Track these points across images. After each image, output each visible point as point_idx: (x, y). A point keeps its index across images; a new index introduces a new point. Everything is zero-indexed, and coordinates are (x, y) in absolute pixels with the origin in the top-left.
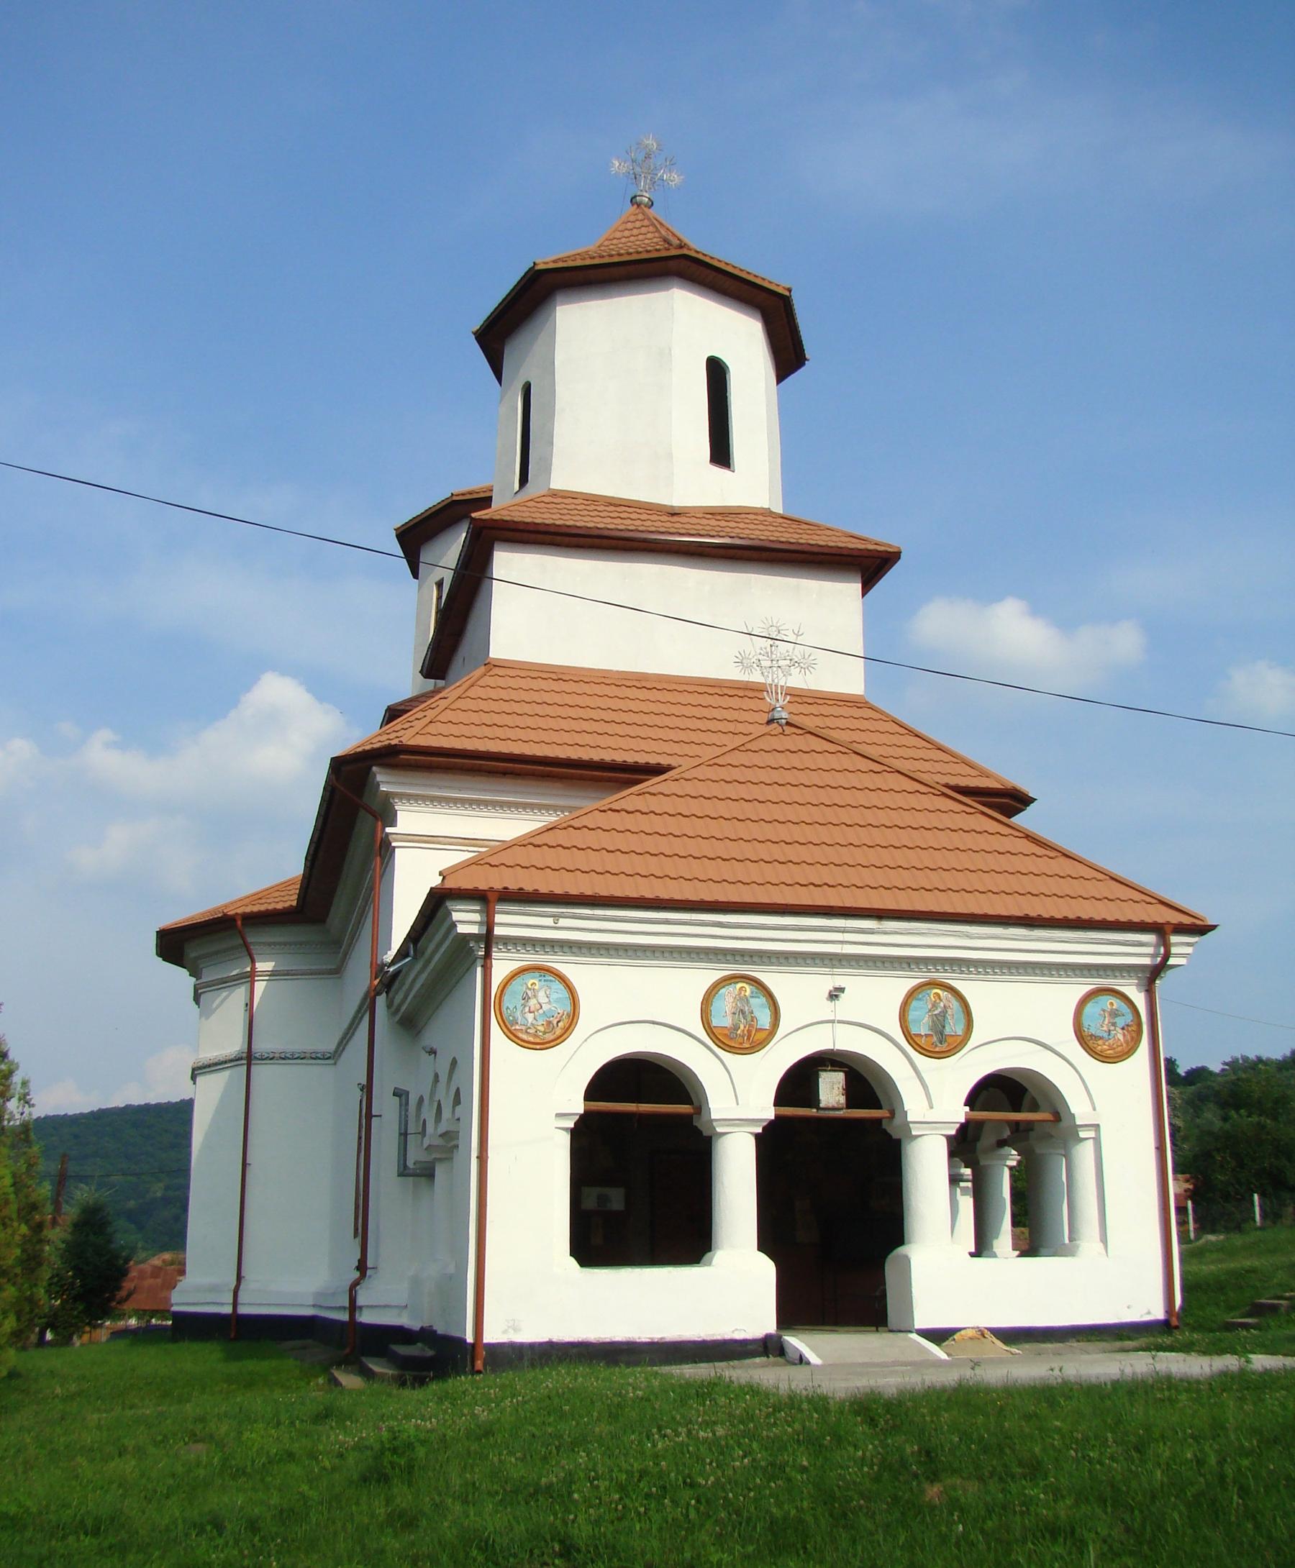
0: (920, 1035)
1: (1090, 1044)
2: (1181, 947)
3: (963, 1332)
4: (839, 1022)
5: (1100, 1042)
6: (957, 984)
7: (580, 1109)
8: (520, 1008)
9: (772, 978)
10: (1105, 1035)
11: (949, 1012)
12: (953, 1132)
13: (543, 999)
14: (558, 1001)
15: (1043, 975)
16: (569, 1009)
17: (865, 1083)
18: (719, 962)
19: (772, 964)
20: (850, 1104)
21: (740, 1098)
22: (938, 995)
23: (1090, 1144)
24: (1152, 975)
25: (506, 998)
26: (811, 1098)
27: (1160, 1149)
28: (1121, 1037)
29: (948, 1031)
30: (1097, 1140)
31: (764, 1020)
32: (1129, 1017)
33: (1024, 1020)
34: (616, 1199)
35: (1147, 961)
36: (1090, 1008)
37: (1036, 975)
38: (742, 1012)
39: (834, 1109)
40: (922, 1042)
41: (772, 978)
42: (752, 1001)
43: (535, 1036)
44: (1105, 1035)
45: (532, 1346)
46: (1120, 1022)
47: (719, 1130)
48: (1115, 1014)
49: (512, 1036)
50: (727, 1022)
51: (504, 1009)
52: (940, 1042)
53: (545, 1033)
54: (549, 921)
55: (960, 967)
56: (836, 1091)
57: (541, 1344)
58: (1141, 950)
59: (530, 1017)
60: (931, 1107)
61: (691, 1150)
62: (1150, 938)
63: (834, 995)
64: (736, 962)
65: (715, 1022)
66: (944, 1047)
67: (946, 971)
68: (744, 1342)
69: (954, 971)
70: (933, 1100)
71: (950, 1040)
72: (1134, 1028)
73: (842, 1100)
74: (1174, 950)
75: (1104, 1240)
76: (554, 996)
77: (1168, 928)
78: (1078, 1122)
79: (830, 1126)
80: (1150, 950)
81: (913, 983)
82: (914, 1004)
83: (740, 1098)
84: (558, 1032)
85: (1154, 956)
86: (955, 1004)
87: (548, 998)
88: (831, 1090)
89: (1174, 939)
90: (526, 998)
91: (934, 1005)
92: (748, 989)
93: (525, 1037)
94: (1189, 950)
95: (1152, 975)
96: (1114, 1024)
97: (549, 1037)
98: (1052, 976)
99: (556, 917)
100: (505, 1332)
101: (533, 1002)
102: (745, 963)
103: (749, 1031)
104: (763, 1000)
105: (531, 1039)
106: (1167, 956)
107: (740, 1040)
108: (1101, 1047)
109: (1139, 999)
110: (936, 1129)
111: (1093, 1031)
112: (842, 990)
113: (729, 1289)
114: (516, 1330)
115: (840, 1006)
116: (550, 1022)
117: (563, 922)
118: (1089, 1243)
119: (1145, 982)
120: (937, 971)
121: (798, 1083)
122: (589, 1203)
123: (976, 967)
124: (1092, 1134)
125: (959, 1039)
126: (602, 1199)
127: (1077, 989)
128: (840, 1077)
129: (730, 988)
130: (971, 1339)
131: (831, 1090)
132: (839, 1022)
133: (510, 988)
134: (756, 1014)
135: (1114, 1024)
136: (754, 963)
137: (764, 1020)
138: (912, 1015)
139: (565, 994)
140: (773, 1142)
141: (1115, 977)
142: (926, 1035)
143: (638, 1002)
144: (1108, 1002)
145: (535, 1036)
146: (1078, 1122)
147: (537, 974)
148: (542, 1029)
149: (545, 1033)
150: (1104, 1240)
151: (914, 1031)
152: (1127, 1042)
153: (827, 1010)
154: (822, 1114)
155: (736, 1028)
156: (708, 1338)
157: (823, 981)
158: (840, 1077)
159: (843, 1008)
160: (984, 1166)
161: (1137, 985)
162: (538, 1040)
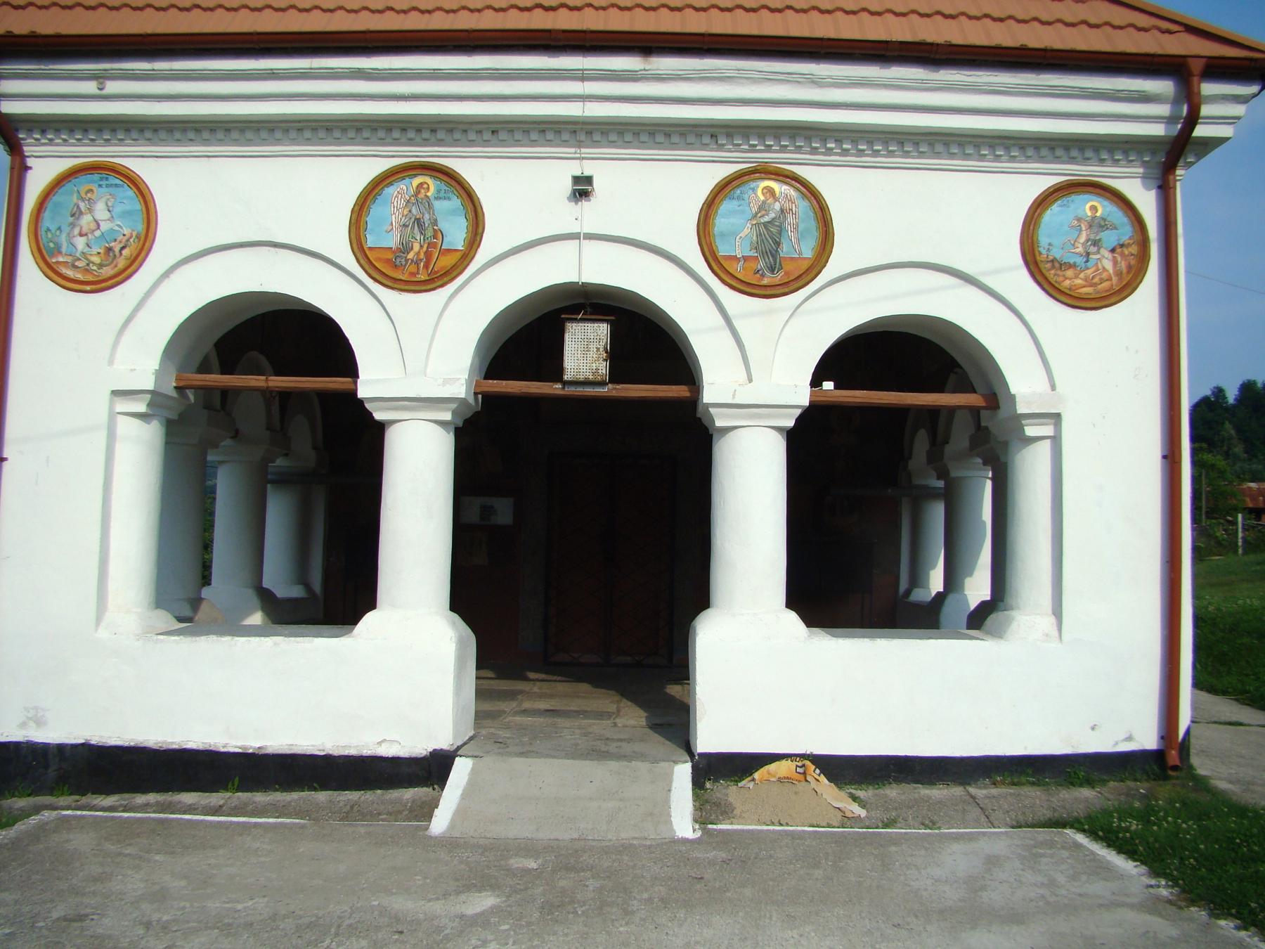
0: (734, 258)
1: (1051, 275)
2: (1225, 109)
3: (773, 767)
4: (590, 237)
5: (1070, 273)
6: (134, 165)
7: (802, 397)
8: (66, 229)
9: (475, 169)
10: (1080, 261)
11: (790, 219)
12: (790, 423)
13: (101, 211)
14: (127, 214)
15: (967, 157)
16: (141, 227)
17: (647, 341)
18: (382, 142)
19: (471, 143)
20: (616, 376)
21: (416, 363)
22: (770, 191)
23: (1044, 448)
24: (1173, 154)
25: (47, 215)
26: (551, 364)
27: (1171, 458)
28: (1108, 265)
29: (785, 250)
30: (1056, 440)
31: (456, 234)
32: (1125, 231)
33: (930, 236)
34: (503, 511)
35: (1158, 130)
36: (1054, 215)
37: (952, 156)
38: (418, 221)
39: (586, 383)
40: (738, 269)
41: (475, 169)
42: (437, 205)
43: (87, 271)
44: (1080, 261)
45: (61, 748)
46: (1110, 238)
47: (718, 423)
48: (1099, 225)
49: (52, 271)
50: (392, 241)
51: (42, 232)
52: (772, 270)
53: (101, 266)
54: (90, 87)
55: (824, 141)
56: (593, 354)
57: (75, 747)
58: (1143, 109)
59: (80, 243)
60: (750, 380)
61: (347, 449)
62: (1163, 86)
63: (582, 189)
64: (411, 142)
65: (371, 241)
66: (779, 277)
67: (783, 149)
68: (395, 761)
69: (798, 149)
70: (757, 372)
71: (788, 266)
72: (1134, 249)
73: (603, 368)
74: (1205, 110)
75: (1057, 612)
76: (119, 209)
77: (1196, 66)
78: (1021, 409)
79: (584, 411)
80: (1164, 110)
81: (723, 171)
82: (726, 207)
83: (416, 363)
84: (121, 263)
85: (1170, 120)
86: (803, 207)
87: (106, 213)
88: (585, 351)
89: (1208, 88)
90: (77, 214)
91: (763, 207)
92: (432, 185)
93: (70, 273)
94: (1238, 110)
95: (1173, 154)
96: (1096, 243)
97: (107, 271)
98: (982, 158)
99: (100, 78)
100: (23, 725)
101: (86, 220)
102: (426, 142)
103: (428, 255)
104: (455, 203)
105: (80, 276)
106: (1193, 119)
107: (417, 268)
108: (1069, 281)
109: (1146, 202)
110: (760, 417)
111: (1057, 253)
112: (588, 180)
113: (400, 668)
114: (40, 722)
115: (592, 209)
116: (109, 250)
117: (112, 87)
118: (1029, 618)
119: (1157, 172)
120: (769, 149)
121: (526, 340)
122: (473, 517)
123: (838, 141)
124: (1048, 430)
125: (805, 265)
126: (487, 511)
127: (1025, 185)
128: (601, 331)
129: (402, 186)
130: (780, 780)
131: (585, 351)
132: (590, 237)
133: (56, 198)
134: (443, 225)
135: (1096, 243)
136: (440, 143)
137: (456, 234)
138: (724, 220)
139: (138, 206)
140: (488, 442)
141: (1102, 162)
142: (745, 258)
143: (255, 215)
144: (1089, 205)
145: (87, 271)
146: (1021, 409)
147: (96, 177)
148: (97, 260)
149: (101, 266)
150: (1057, 612)
151: (723, 250)
152: (1119, 274)
153: (568, 217)
154: (570, 390)
155: (405, 248)
156: (336, 753)
157: (550, 173)
158: (601, 331)
159: (591, 216)
160: (960, 478)
161: (1144, 177)
162: (90, 278)
